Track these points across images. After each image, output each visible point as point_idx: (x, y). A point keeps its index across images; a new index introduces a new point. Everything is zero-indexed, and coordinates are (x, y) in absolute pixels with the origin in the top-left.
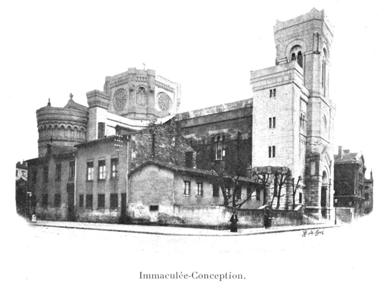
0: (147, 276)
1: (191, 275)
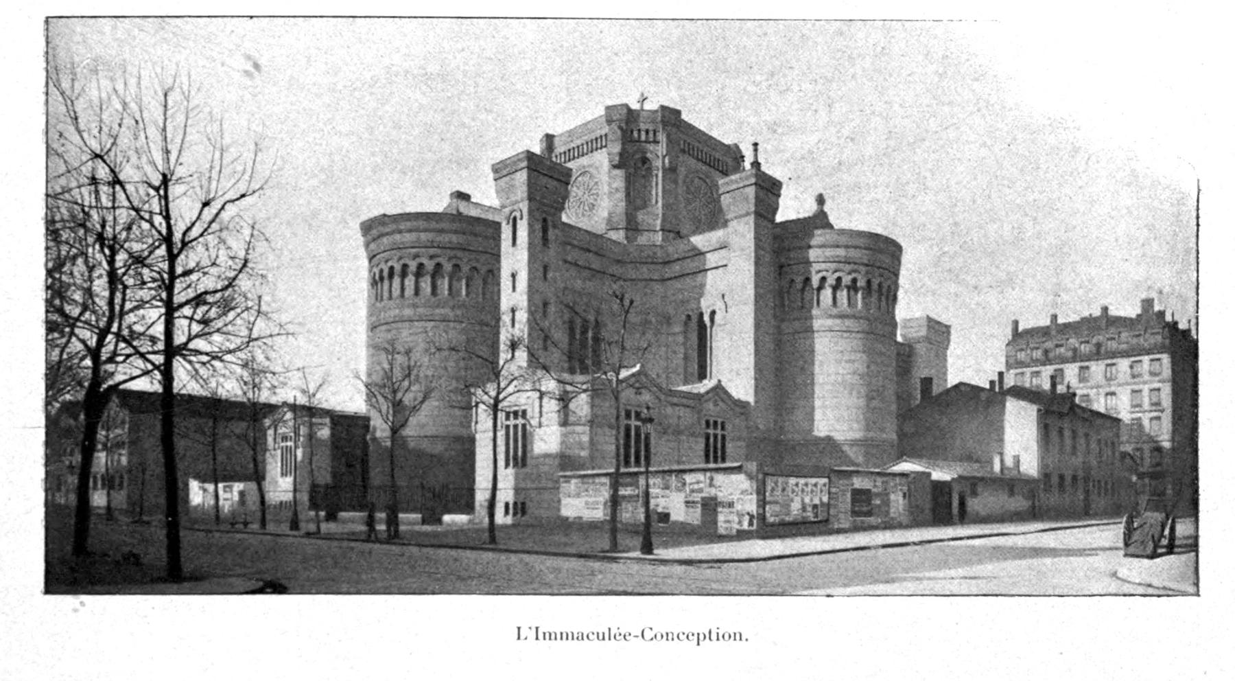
0: (550, 636)
1: (640, 635)
